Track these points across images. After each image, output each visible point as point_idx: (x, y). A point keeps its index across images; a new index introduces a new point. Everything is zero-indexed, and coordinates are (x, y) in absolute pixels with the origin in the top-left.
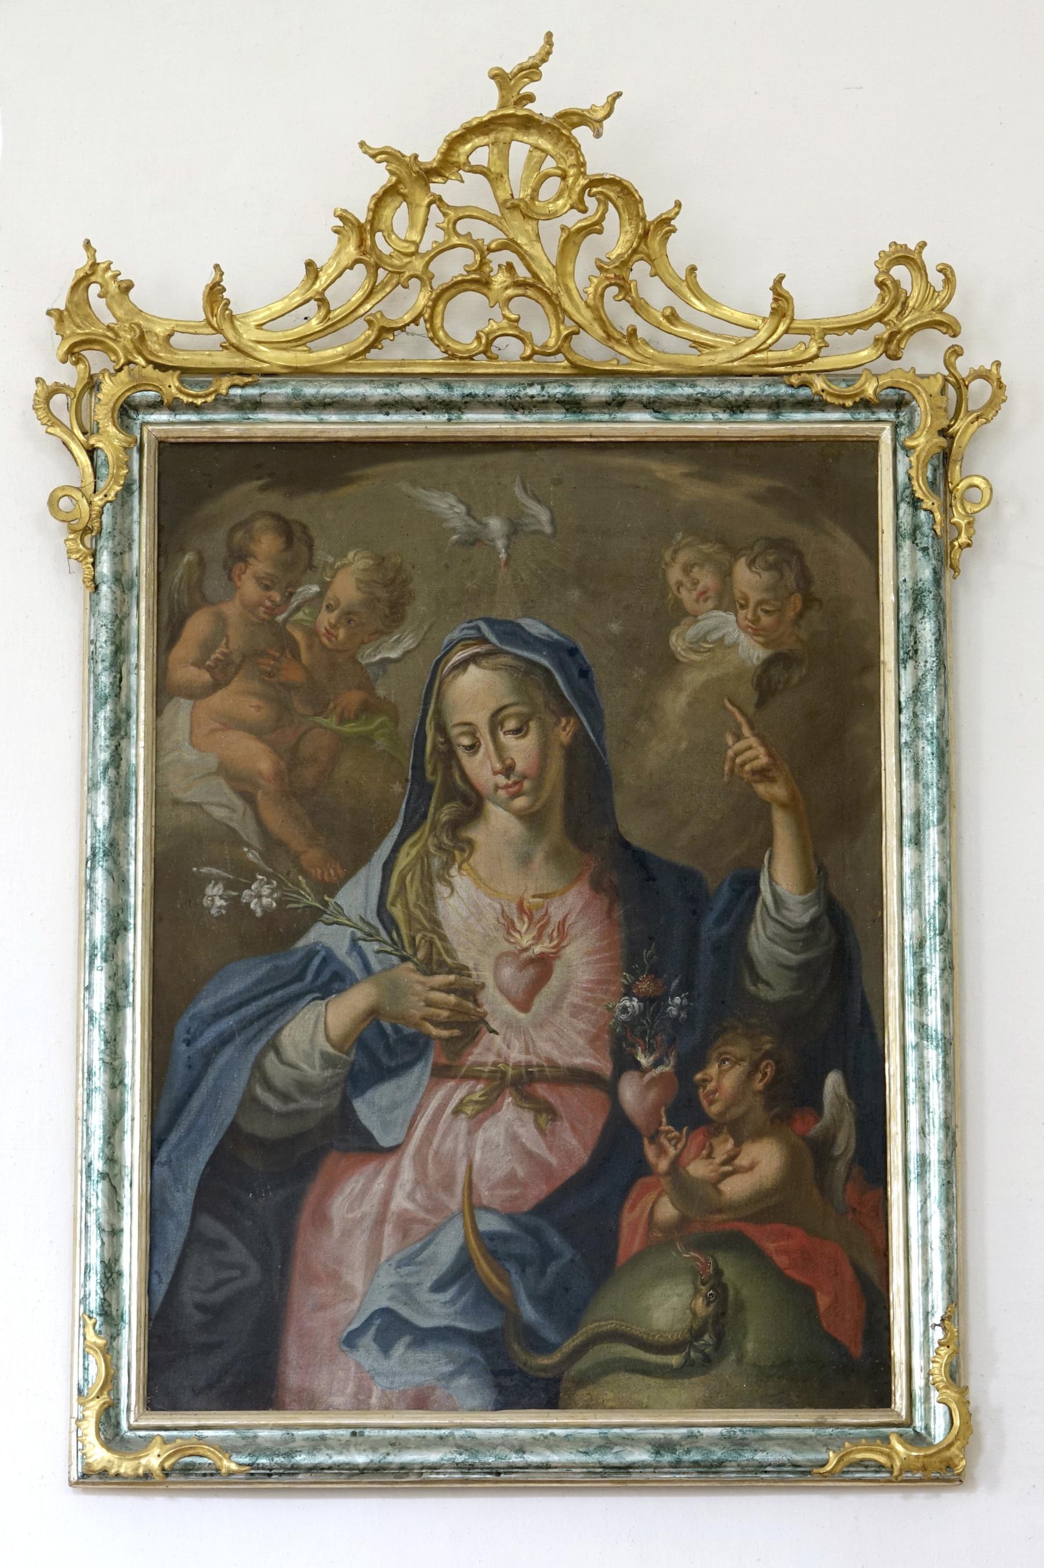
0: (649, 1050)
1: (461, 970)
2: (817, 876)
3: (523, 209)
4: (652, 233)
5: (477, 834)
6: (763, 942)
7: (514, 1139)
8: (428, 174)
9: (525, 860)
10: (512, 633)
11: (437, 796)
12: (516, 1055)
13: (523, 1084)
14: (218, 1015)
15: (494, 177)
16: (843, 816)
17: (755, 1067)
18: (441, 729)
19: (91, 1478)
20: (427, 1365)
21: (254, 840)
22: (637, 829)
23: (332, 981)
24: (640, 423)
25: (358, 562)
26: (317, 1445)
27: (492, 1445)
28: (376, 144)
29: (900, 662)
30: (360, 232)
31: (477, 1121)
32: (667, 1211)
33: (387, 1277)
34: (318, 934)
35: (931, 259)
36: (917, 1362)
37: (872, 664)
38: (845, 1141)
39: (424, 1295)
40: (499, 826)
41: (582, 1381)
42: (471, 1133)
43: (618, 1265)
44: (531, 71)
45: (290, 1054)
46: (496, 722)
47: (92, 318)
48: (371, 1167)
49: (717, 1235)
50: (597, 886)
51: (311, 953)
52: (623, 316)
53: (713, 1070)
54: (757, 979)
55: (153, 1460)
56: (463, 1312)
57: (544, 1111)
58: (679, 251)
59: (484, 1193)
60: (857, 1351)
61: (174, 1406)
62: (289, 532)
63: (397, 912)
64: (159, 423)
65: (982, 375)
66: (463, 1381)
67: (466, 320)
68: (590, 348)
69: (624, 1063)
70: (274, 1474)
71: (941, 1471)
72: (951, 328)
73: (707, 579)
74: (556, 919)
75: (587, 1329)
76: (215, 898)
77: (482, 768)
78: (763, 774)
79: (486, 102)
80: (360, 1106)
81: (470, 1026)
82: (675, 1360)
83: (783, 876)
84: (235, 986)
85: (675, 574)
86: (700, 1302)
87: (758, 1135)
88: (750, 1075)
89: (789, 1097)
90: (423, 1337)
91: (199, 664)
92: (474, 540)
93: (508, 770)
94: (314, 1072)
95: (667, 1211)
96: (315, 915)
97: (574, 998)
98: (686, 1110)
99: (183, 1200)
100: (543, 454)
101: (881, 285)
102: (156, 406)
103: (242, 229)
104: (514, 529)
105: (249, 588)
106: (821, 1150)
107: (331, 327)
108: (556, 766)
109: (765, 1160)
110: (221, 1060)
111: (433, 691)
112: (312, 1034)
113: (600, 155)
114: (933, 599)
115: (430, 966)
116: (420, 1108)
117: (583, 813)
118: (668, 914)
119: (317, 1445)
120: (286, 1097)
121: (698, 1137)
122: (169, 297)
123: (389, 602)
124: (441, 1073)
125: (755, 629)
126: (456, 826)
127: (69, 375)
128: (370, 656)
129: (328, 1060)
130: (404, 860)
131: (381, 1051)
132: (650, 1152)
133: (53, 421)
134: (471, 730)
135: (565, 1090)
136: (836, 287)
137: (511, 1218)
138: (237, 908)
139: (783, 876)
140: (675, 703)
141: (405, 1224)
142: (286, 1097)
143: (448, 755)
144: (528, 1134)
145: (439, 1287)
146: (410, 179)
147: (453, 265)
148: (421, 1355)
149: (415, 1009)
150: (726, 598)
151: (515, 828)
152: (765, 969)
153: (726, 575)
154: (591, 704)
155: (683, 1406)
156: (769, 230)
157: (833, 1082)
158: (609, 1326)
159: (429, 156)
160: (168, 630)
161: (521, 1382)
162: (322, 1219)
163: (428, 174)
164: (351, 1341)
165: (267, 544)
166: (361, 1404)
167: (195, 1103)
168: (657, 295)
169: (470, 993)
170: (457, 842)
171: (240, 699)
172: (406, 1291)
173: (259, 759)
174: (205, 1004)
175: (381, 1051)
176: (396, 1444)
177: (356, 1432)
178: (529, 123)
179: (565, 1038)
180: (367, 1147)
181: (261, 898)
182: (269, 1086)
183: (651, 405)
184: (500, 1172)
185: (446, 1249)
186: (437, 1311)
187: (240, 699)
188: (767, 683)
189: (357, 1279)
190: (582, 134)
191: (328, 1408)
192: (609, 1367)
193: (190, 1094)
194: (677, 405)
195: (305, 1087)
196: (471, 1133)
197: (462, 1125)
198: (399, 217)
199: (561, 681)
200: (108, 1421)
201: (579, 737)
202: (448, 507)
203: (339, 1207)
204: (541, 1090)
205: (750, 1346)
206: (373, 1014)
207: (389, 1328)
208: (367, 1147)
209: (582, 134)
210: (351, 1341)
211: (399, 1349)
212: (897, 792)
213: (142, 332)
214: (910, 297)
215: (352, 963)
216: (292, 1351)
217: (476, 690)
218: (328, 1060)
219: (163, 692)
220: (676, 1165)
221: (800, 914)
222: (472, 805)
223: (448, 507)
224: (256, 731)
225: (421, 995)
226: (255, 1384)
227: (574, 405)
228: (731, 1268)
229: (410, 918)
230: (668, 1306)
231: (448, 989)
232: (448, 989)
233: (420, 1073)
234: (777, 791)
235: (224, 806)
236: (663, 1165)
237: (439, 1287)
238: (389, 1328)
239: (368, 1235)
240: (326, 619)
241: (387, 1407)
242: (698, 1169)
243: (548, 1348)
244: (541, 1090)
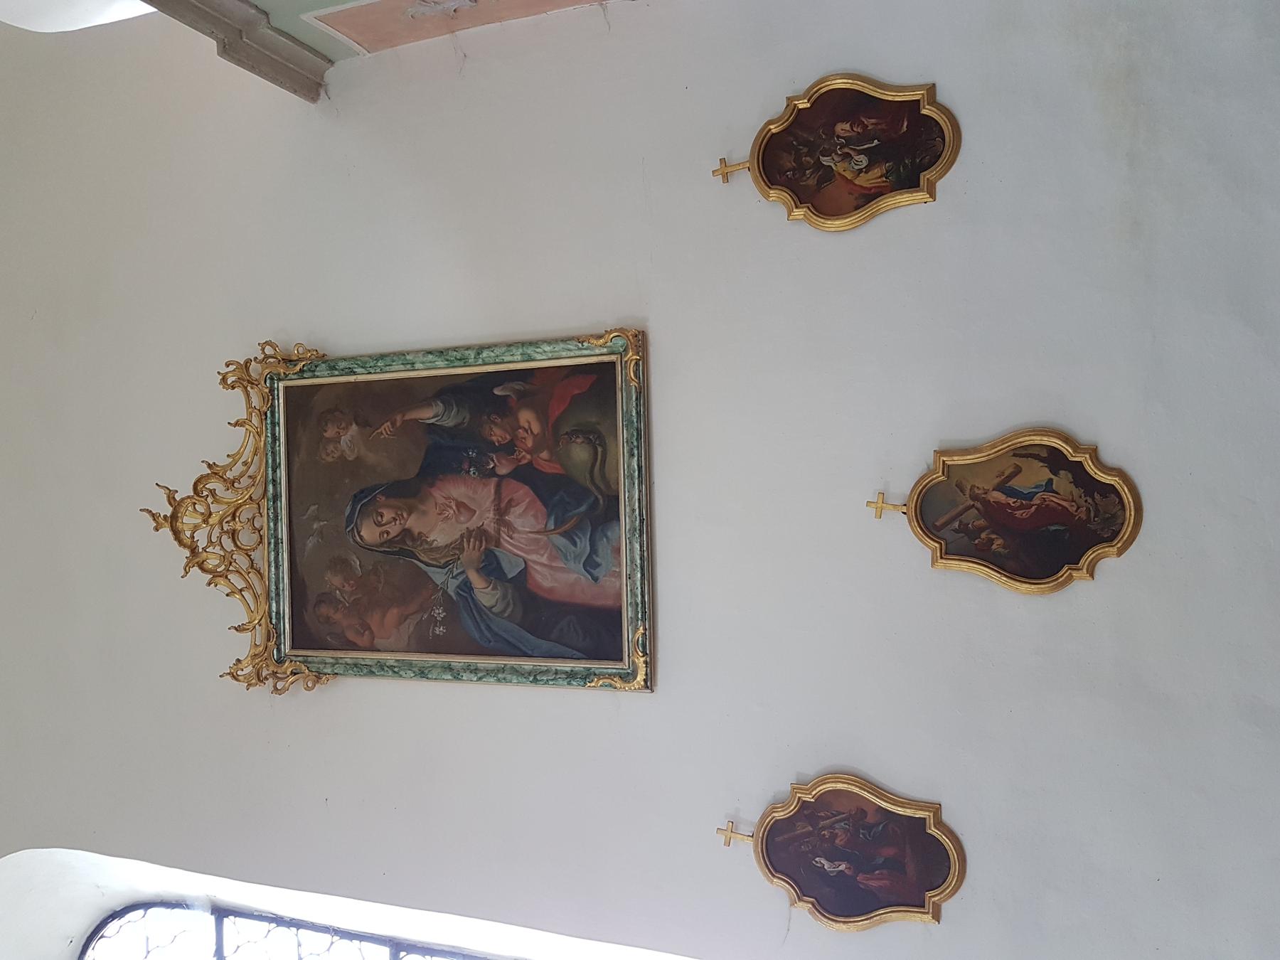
0: (488, 464)
1: (462, 536)
2: (426, 402)
3: (207, 517)
4: (215, 471)
5: (416, 531)
6: (449, 422)
7: (520, 516)
8: (194, 551)
9: (424, 513)
10: (350, 520)
11: (403, 547)
12: (491, 515)
13: (501, 511)
14: (481, 631)
15: (196, 528)
16: (405, 394)
17: (493, 422)
18: (382, 545)
19: (649, 684)
20: (603, 547)
21: (419, 616)
22: (413, 471)
23: (467, 586)
24: (282, 473)
25: (328, 576)
26: (634, 595)
27: (633, 522)
28: (183, 573)
29: (355, 373)
30: (215, 575)
31: (515, 530)
32: (545, 455)
33: (572, 565)
34: (451, 592)
35: (224, 370)
36: (597, 352)
37: (356, 384)
38: (518, 386)
39: (578, 550)
40: (413, 523)
41: (608, 485)
42: (519, 532)
43: (562, 472)
44: (154, 516)
45: (492, 602)
46: (379, 525)
47: (267, 669)
48: (533, 572)
49: (553, 436)
50: (432, 485)
51: (458, 594)
52: (245, 481)
53: (494, 438)
54: (463, 423)
55: (640, 661)
56: (584, 535)
57: (510, 504)
58: (222, 461)
59: (541, 527)
60: (595, 377)
61: (621, 651)
62: (319, 602)
63: (443, 561)
64: (286, 647)
65: (263, 350)
66: (609, 534)
67: (246, 538)
68: (256, 492)
69: (493, 473)
70: (648, 612)
71: (640, 341)
72: (248, 362)
73: (331, 447)
74: (443, 501)
75: (588, 484)
76: (440, 630)
77: (394, 530)
78: (393, 424)
79: (166, 531)
80: (510, 576)
81: (481, 533)
82: (600, 449)
83: (427, 415)
84: (469, 622)
85: (329, 459)
86: (579, 440)
87: (517, 420)
88: (496, 424)
89: (503, 408)
90: (594, 550)
91: (363, 635)
92: (321, 533)
93: (395, 519)
94: (499, 594)
95: (545, 455)
96: (445, 592)
97: (470, 493)
98: (509, 449)
99: (545, 645)
100: (293, 509)
101: (233, 388)
102: (279, 650)
103: (218, 621)
104: (317, 519)
105: (338, 617)
106: (522, 395)
107: (250, 587)
108: (392, 501)
109: (526, 417)
110: (496, 629)
111: (369, 548)
112: (486, 595)
113: (185, 491)
114: (332, 365)
115: (462, 550)
116: (511, 552)
117: (407, 492)
118: (443, 457)
119: (634, 595)
120: (508, 605)
121: (518, 443)
122: (242, 646)
123: (341, 565)
124: (498, 544)
125: (346, 428)
126: (413, 539)
127: (270, 682)
128: (359, 572)
129: (494, 588)
130: (426, 559)
131: (491, 567)
132: (524, 462)
133: (285, 690)
134: (382, 534)
135: (503, 495)
136: (236, 403)
137: (549, 516)
138: (442, 623)
139: (427, 415)
140: (371, 458)
141: (551, 558)
142: (508, 605)
143: (390, 542)
144: (518, 510)
145: (575, 544)
146: (195, 558)
147: (228, 543)
148: (600, 551)
149: (476, 554)
150: (337, 440)
151: (413, 517)
152: (459, 420)
153: (329, 440)
154: (373, 489)
155: (617, 445)
156: (215, 430)
157: (497, 392)
158: (588, 476)
159: (187, 553)
160: (354, 647)
161: (608, 512)
162: (551, 590)
163: (194, 551)
164: (596, 579)
165: (324, 610)
166: (619, 575)
167: (511, 640)
168: (238, 468)
169: (469, 532)
170: (420, 538)
171: (374, 620)
172: (577, 557)
173: (393, 614)
174: (477, 636)
175: (491, 567)
176: (633, 560)
177: (629, 577)
178: (174, 518)
179: (482, 496)
180: (525, 572)
181: (439, 613)
182: (504, 611)
183: (274, 471)
184: (532, 520)
185: (561, 541)
186: (584, 545)
187: (374, 620)
188: (364, 424)
189: (573, 577)
190: (178, 497)
191: (621, 588)
192: (603, 476)
193: (509, 643)
194: (274, 460)
195: (504, 597)
196: (519, 532)
197: (515, 535)
198: (212, 562)
199: (365, 500)
200: (628, 677)
201: (382, 493)
202: (311, 543)
203: (547, 583)
204: (503, 505)
205: (594, 420)
206: (478, 571)
207: (590, 564)
208: (525, 572)
209: (178, 497)
210: (596, 579)
211: (598, 560)
212: (398, 373)
213: (526, 567)
214: (240, 376)
215: (461, 578)
216: (599, 603)
217: (369, 533)
218: (494, 588)
219: (373, 649)
220: (528, 452)
221: (439, 407)
222: (406, 532)
223: (311, 543)
224: (384, 616)
225: (471, 553)
226: (614, 616)
227: (276, 497)
228: (566, 429)
229: (445, 556)
230: (580, 453)
231: (469, 542)
232: (469, 542)
233: (498, 552)
234: (399, 418)
235: (409, 627)
236: (528, 457)
237: (575, 544)
238: (590, 564)
239: (556, 574)
240: (347, 588)
241: (620, 565)
242: (530, 443)
243: (597, 499)
244: (503, 505)
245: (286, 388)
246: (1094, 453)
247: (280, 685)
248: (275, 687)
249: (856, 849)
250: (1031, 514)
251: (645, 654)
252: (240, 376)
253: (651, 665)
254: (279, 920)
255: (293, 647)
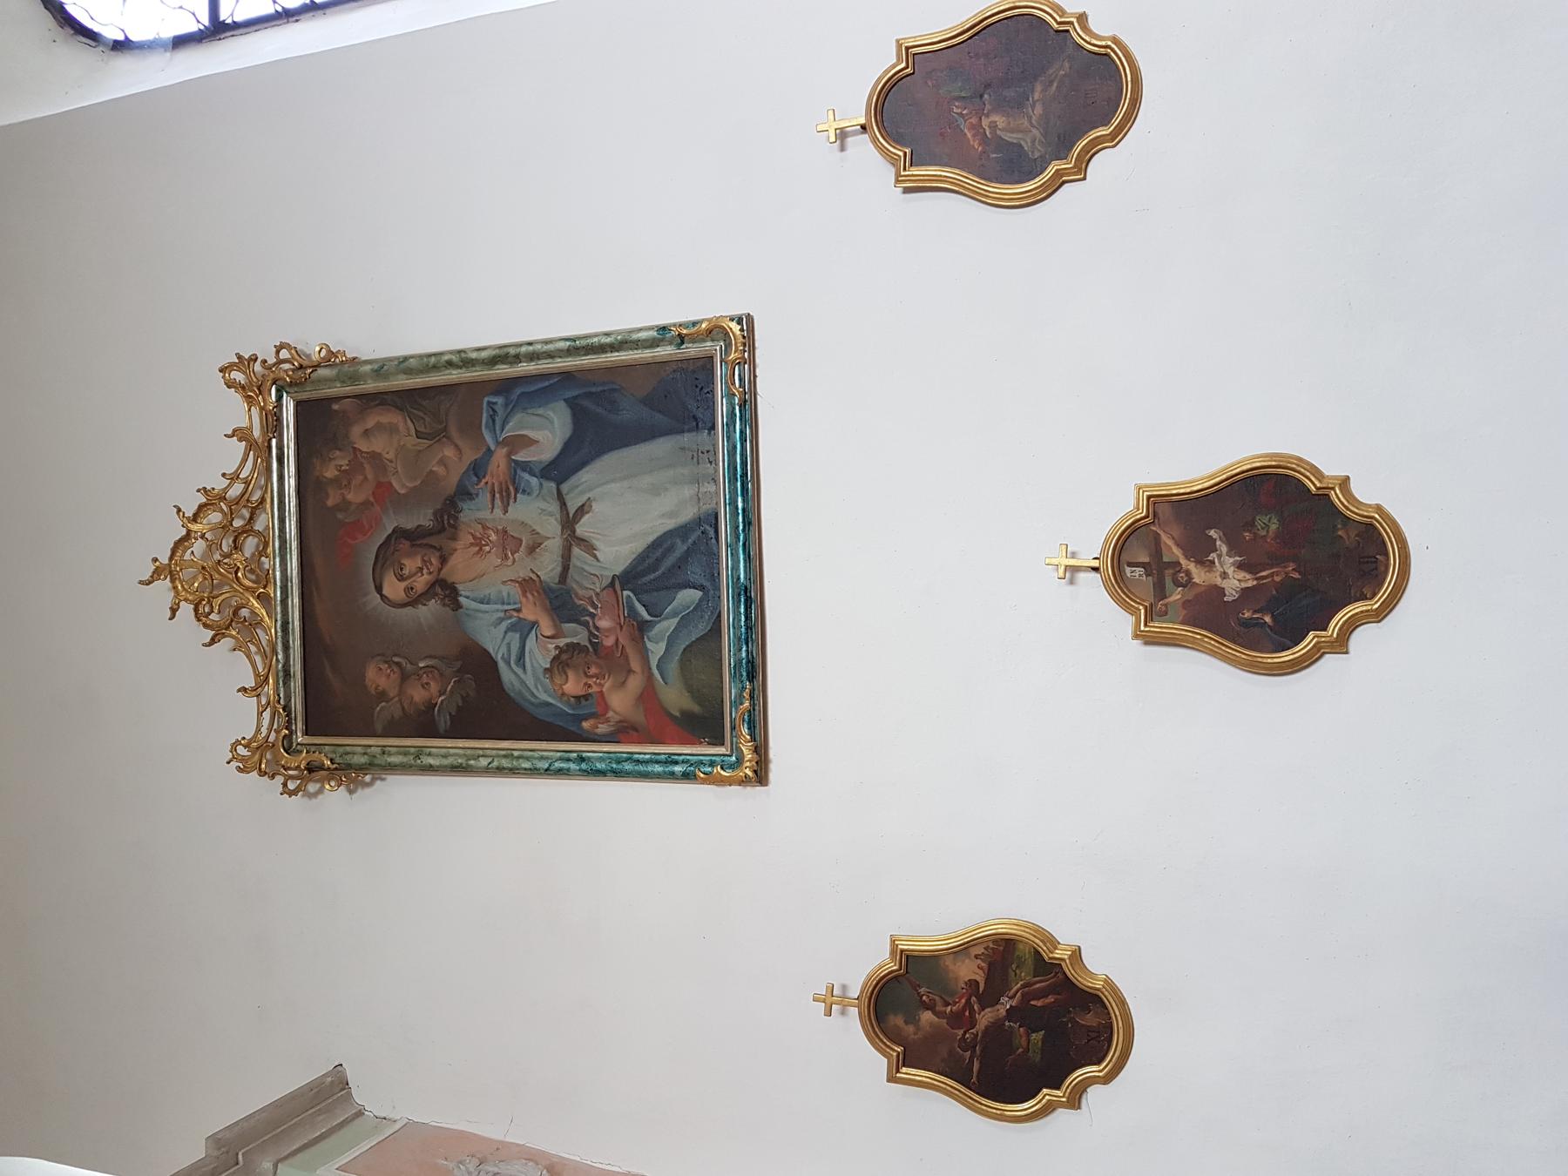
19: (760, 776)
28: (169, 613)
65: (278, 352)
122: (245, 719)
136: (237, 412)
191: (718, 503)
245: (306, 733)
246: (1379, 615)
247: (291, 785)
248: (285, 785)
249: (1006, 1021)
250: (1269, 564)
251: (753, 739)
252: (251, 378)
253: (761, 750)
254: (287, 15)
255: (306, 733)
